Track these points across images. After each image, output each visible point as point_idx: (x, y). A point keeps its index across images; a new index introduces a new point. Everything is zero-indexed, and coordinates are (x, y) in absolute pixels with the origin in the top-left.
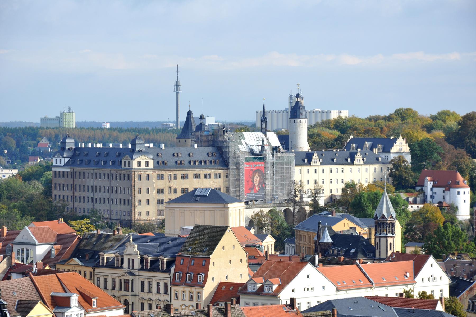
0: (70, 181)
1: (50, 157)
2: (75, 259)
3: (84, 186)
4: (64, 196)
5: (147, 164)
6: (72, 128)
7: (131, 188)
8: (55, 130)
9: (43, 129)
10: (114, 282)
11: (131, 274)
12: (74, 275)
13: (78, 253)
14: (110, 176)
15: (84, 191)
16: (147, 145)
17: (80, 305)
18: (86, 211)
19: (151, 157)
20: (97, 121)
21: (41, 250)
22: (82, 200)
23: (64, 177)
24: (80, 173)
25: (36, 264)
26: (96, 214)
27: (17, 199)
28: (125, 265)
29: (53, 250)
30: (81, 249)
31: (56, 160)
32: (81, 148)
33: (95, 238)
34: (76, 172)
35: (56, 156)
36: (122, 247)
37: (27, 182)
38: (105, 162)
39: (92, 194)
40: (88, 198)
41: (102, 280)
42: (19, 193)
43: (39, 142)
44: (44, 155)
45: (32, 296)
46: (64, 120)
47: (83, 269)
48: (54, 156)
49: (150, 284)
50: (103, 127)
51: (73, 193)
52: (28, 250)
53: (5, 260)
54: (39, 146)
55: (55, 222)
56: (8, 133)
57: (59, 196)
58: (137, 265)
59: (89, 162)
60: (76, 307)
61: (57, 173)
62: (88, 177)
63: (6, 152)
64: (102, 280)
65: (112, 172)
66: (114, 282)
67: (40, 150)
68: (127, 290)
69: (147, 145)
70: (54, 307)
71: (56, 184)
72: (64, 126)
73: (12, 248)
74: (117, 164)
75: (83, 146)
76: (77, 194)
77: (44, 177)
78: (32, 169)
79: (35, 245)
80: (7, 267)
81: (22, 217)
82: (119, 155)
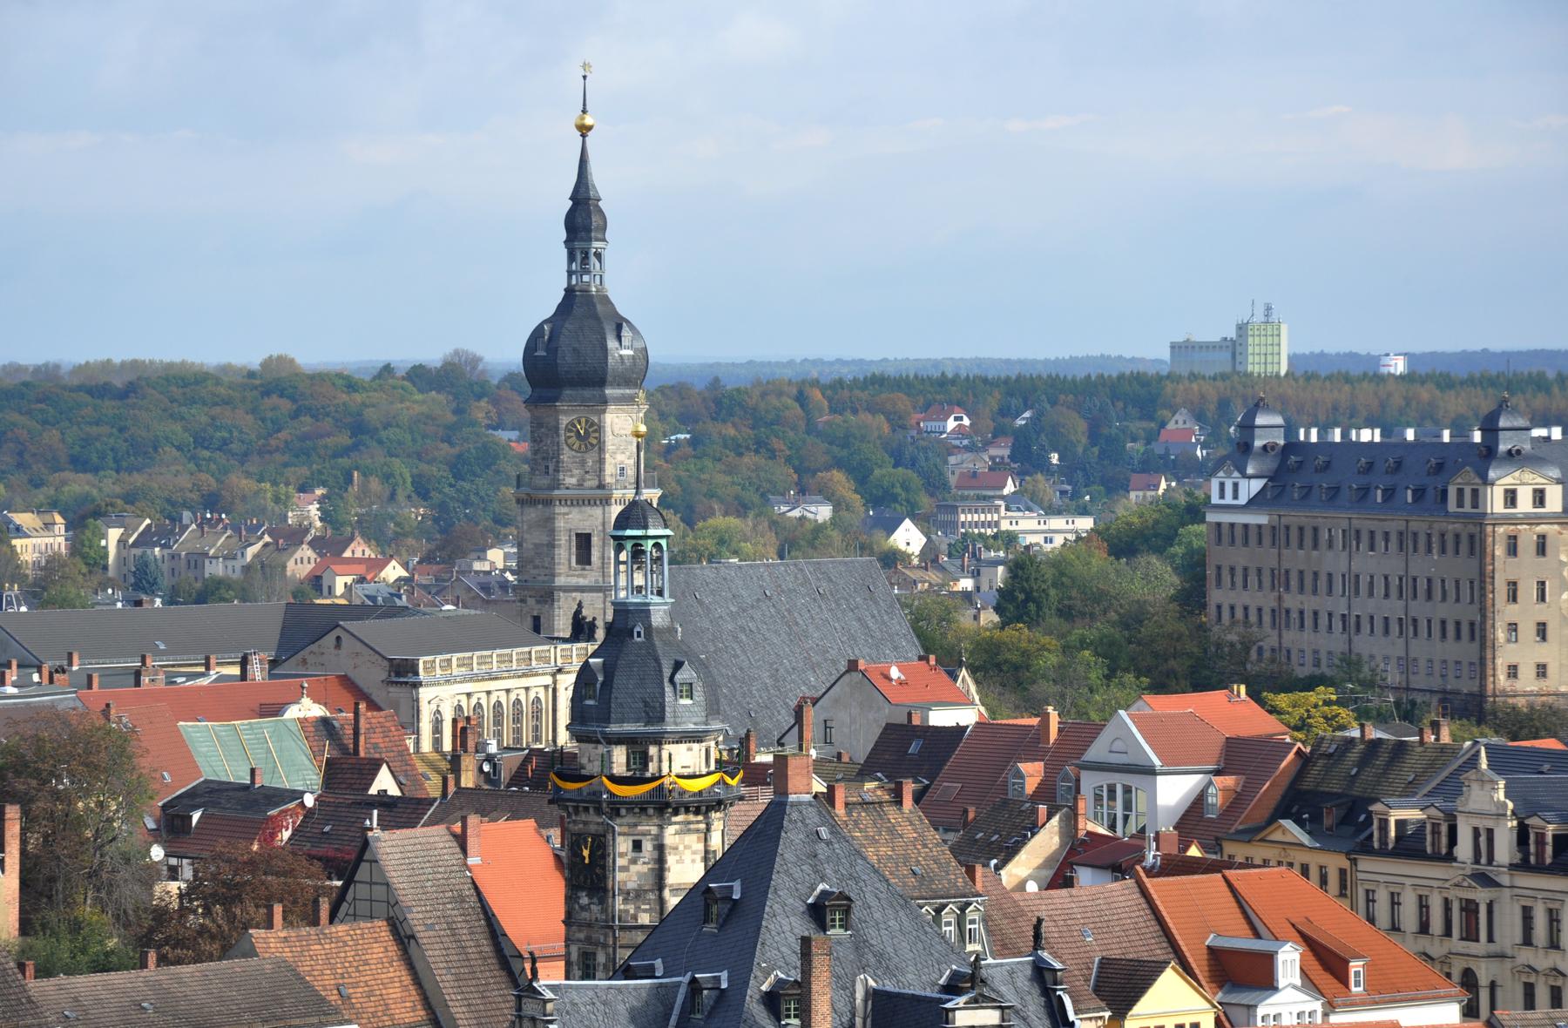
0: (1267, 557)
2: (1288, 824)
4: (1246, 608)
5: (1539, 497)
6: (1278, 375)
7: (1481, 583)
10: (1423, 906)
11: (1485, 880)
12: (1286, 878)
13: (1298, 802)
14: (1407, 542)
15: (1315, 592)
16: (1538, 432)
17: (1309, 983)
19: (1555, 473)
20: (1363, 353)
21: (1173, 791)
22: (1308, 622)
23: (1246, 543)
24: (1301, 529)
25: (1157, 839)
28: (1464, 849)
31: (1222, 485)
33: (1354, 755)
35: (1221, 474)
36: (1452, 788)
38: (1389, 494)
39: (1344, 601)
40: (1330, 615)
41: (1382, 897)
42: (1099, 597)
43: (1163, 425)
44: (1182, 467)
45: (1147, 947)
46: (1250, 350)
47: (1314, 860)
48: (1213, 473)
49: (1395, 902)
50: (1384, 370)
51: (1280, 598)
52: (1127, 790)
53: (1055, 820)
55: (1218, 696)
56: (1062, 397)
57: (1232, 608)
58: (1505, 849)
59: (1334, 492)
60: (1295, 987)
61: (1225, 531)
62: (1330, 545)
63: (1055, 458)
64: (1382, 897)
65: (1414, 526)
66: (1423, 906)
68: (1471, 935)
69: (1538, 432)
70: (1220, 987)
71: (1219, 568)
72: (1250, 368)
73: (1078, 780)
74: (1431, 498)
75: (1314, 438)
76: (1292, 601)
77: (1180, 544)
79: (1151, 772)
80: (1062, 845)
81: (1108, 677)
82: (1440, 467)
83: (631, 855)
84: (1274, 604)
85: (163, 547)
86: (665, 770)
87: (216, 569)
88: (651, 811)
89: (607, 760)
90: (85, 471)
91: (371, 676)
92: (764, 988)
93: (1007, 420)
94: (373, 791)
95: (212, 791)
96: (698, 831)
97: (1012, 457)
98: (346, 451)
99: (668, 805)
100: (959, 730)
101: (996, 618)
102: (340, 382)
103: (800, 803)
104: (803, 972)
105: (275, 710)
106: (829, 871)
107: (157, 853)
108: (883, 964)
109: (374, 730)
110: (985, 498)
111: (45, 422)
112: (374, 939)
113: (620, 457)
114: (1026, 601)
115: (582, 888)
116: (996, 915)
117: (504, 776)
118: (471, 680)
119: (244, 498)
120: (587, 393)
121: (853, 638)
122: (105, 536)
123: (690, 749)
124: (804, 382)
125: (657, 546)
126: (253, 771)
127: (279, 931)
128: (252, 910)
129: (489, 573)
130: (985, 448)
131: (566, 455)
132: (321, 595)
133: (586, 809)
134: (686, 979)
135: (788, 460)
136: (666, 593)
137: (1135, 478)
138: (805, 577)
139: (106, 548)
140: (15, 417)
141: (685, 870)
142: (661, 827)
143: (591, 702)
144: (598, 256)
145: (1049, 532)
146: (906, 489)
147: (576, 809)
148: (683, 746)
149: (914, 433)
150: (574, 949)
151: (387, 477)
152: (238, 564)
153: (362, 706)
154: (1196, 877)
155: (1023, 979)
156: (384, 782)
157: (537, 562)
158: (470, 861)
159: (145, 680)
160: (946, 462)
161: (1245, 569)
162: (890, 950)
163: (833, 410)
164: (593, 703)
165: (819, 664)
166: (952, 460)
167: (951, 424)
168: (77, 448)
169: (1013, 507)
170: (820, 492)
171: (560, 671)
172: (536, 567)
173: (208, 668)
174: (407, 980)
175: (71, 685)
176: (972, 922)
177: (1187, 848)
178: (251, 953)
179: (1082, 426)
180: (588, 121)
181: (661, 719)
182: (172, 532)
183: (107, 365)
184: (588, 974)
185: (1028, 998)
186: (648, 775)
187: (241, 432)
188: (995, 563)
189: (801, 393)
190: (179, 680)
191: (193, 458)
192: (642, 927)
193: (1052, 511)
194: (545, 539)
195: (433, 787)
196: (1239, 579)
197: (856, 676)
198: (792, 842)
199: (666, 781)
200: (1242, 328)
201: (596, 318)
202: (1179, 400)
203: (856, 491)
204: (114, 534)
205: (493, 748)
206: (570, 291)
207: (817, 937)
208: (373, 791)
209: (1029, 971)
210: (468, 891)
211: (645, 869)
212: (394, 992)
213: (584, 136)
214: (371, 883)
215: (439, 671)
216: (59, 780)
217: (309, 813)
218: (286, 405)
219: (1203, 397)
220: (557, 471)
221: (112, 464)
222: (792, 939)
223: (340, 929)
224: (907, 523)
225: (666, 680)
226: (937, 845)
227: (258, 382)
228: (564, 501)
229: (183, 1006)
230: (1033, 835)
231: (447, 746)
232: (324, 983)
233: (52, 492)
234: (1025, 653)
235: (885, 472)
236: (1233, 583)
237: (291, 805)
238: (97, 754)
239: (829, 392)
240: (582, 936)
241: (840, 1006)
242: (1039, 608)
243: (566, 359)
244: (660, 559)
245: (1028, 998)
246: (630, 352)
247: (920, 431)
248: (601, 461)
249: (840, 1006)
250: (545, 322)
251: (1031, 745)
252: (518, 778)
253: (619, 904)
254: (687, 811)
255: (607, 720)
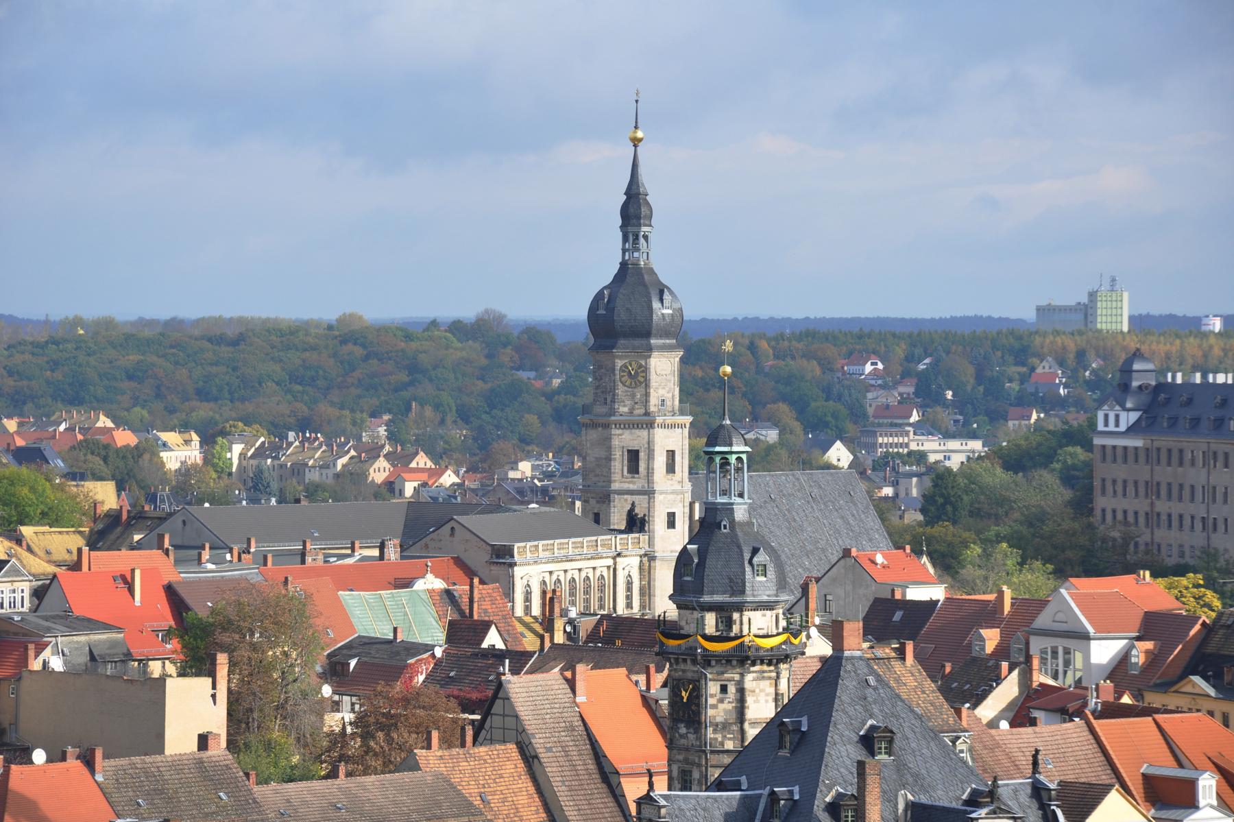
0: (1143, 472)
1: (1063, 408)
2: (1197, 679)
3: (1181, 486)
4: (1125, 512)
6: (1122, 332)
8: (1078, 338)
9: (1045, 335)
15: (1180, 499)
18: (1187, 554)
20: (1181, 314)
21: (1103, 652)
22: (1175, 523)
23: (1125, 461)
24: (1169, 451)
25: (1097, 689)
26: (1216, 561)
27: (997, 517)
29: (1134, 652)
30: (1210, 655)
31: (1106, 416)
32: (1173, 385)
34: (1158, 450)
35: (1106, 407)
37: (1021, 474)
39: (1203, 507)
40: (1193, 517)
42: (1002, 501)
43: (1033, 369)
45: (1096, 773)
46: (1099, 312)
48: (1099, 408)
50: (1204, 328)
51: (1152, 504)
52: (1067, 652)
53: (1016, 673)
54: (1033, 380)
55: (1129, 579)
56: (954, 347)
57: (1114, 511)
60: (1212, 807)
61: (1109, 452)
62: (1193, 463)
65: (1213, 447)
67: (1037, 392)
70: (1153, 805)
71: (1104, 480)
72: (1099, 326)
73: (1027, 644)
75: (1179, 380)
76: (1162, 506)
77: (1058, 461)
78: (1027, 439)
79: (1086, 637)
80: (1021, 693)
81: (1021, 564)
83: (719, 696)
84: (1148, 509)
85: (274, 458)
86: (745, 632)
87: (313, 476)
88: (734, 663)
89: (701, 623)
90: (208, 401)
91: (478, 558)
92: (828, 799)
93: (912, 365)
94: (485, 645)
95: (365, 644)
96: (770, 678)
97: (917, 394)
98: (405, 386)
99: (747, 658)
100: (932, 604)
101: (920, 517)
102: (399, 333)
103: (853, 658)
104: (859, 788)
105: (406, 583)
106: (876, 711)
107: (327, 690)
108: (918, 782)
109: (484, 600)
110: (896, 425)
111: (176, 363)
112: (507, 757)
113: (661, 392)
114: (943, 505)
115: (682, 721)
116: (978, 746)
117: (582, 634)
118: (553, 562)
119: (329, 422)
120: (637, 342)
121: (838, 531)
122: (230, 450)
123: (764, 615)
124: (753, 335)
125: (739, 459)
126: (395, 629)
127: (436, 750)
128: (406, 735)
129: (521, 480)
130: (894, 387)
131: (621, 390)
132: (394, 497)
133: (685, 661)
134: (766, 791)
135: (744, 395)
136: (746, 496)
137: (1013, 411)
138: (800, 484)
139: (231, 459)
140: (155, 358)
141: (761, 709)
142: (742, 675)
143: (688, 579)
144: (646, 238)
145: (954, 453)
146: (836, 417)
147: (677, 660)
148: (759, 613)
149: (840, 375)
150: (675, 768)
151: (437, 407)
152: (330, 472)
153: (476, 581)
154: (1132, 719)
155: (1025, 796)
156: (493, 639)
157: (598, 471)
158: (578, 699)
159: (309, 559)
160: (865, 397)
161: (1125, 482)
162: (923, 771)
163: (777, 357)
164: (690, 576)
165: (812, 551)
166: (870, 395)
167: (868, 368)
168: (201, 383)
169: (919, 432)
170: (769, 420)
171: (619, 555)
172: (597, 476)
173: (353, 551)
174: (532, 790)
175: (254, 563)
176: (962, 751)
177: (1120, 697)
178: (415, 767)
179: (971, 370)
180: (640, 134)
181: (743, 592)
182: (281, 447)
183: (218, 321)
184: (684, 789)
185: (1029, 811)
186: (732, 634)
187: (325, 372)
188: (910, 475)
189: (752, 343)
190: (332, 560)
191: (289, 391)
192: (728, 751)
193: (948, 435)
194: (603, 454)
195: (530, 643)
196: (1119, 488)
197: (850, 561)
198: (847, 688)
199: (746, 639)
200: (1093, 295)
201: (645, 285)
202: (1045, 350)
203: (797, 419)
204: (237, 448)
205: (573, 614)
206: (624, 265)
207: (868, 760)
208: (485, 645)
209: (1029, 791)
210: (578, 723)
211: (730, 707)
212: (523, 799)
213: (635, 146)
214: (504, 715)
215: (529, 554)
216: (252, 635)
217: (438, 663)
218: (359, 351)
219: (1064, 348)
220: (613, 401)
221: (227, 395)
222: (848, 762)
223: (482, 750)
224: (838, 444)
225: (746, 563)
226: (933, 691)
227: (337, 333)
228: (619, 425)
229: (367, 807)
230: (998, 684)
231: (536, 610)
232: (471, 791)
233: (183, 416)
234: (950, 544)
235: (818, 405)
236: (1115, 492)
237: (425, 656)
238: (284, 616)
239: (773, 343)
240: (681, 757)
241: (886, 814)
242: (955, 509)
243: (621, 316)
244: (742, 469)
245: (1029, 811)
246: (670, 311)
247: (844, 373)
248: (647, 395)
249: (886, 814)
250: (605, 288)
251: (989, 614)
252: (593, 636)
253: (710, 733)
254: (762, 663)
255: (701, 593)
